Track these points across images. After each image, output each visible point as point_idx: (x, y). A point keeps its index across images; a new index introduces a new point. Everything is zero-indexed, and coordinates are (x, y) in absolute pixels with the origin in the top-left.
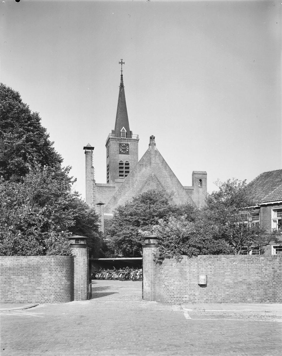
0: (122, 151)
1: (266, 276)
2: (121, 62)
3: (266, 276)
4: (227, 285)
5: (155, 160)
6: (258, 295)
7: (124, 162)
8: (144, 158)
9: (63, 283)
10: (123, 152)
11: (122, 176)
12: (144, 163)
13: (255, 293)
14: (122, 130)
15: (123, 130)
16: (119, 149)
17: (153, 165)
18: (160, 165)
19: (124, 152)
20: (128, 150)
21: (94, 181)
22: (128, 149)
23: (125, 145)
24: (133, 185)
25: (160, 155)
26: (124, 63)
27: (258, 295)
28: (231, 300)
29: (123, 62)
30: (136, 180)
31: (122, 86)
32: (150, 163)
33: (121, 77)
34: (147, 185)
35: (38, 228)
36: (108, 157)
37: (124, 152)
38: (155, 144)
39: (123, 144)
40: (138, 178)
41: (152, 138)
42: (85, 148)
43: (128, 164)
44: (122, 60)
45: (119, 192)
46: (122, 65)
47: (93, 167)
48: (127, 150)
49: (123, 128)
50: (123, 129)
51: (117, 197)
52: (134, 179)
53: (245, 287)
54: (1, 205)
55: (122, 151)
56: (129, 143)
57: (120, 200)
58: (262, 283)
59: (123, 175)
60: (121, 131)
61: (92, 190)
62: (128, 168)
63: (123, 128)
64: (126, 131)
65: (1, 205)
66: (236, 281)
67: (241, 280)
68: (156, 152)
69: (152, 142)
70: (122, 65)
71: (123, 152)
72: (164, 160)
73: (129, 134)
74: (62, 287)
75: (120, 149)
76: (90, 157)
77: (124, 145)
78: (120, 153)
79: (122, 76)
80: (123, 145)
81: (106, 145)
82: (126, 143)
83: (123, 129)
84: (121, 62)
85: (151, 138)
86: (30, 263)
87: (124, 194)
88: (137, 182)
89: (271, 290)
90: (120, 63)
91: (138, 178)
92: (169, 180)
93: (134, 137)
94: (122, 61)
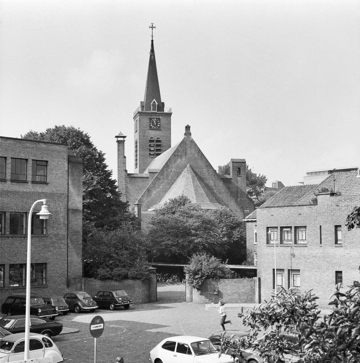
0: (153, 127)
2: (151, 26)
4: (228, 294)
5: (190, 152)
6: (244, 299)
8: (179, 149)
12: (179, 154)
13: (242, 298)
16: (149, 125)
17: (189, 155)
18: (196, 155)
21: (126, 171)
22: (159, 124)
24: (168, 177)
25: (196, 145)
26: (155, 27)
27: (244, 299)
29: (154, 26)
30: (171, 171)
32: (186, 153)
33: (151, 42)
37: (155, 127)
38: (190, 134)
40: (173, 170)
41: (188, 128)
42: (117, 137)
44: (152, 24)
45: (153, 184)
46: (152, 29)
47: (125, 157)
48: (159, 126)
49: (154, 100)
52: (169, 170)
53: (237, 295)
55: (153, 127)
56: (161, 118)
57: (155, 192)
58: (246, 293)
60: (151, 104)
61: (123, 181)
63: (154, 100)
64: (157, 104)
66: (233, 292)
68: (192, 141)
70: (152, 29)
71: (154, 127)
72: (200, 150)
73: (161, 106)
74: (145, 295)
76: (121, 147)
78: (151, 128)
79: (152, 41)
84: (151, 26)
85: (186, 127)
86: (129, 283)
87: (159, 187)
89: (250, 297)
90: (150, 27)
91: (173, 170)
92: (205, 170)
93: (166, 110)
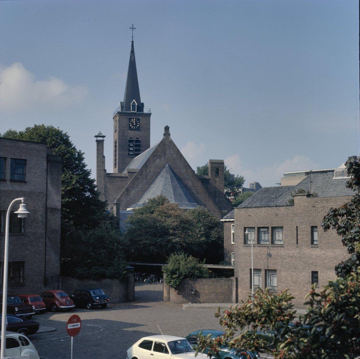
1: (225, 290)
2: (132, 27)
3: (225, 290)
9: (123, 292)
10: (133, 127)
14: (132, 102)
16: (128, 125)
19: (134, 128)
21: (105, 170)
22: (139, 125)
24: (147, 177)
28: (208, 301)
31: (133, 52)
34: (161, 177)
36: (115, 132)
40: (152, 169)
41: (167, 128)
42: (96, 136)
44: (133, 25)
46: (133, 30)
50: (133, 102)
51: (130, 189)
52: (148, 171)
56: (140, 118)
57: (133, 192)
63: (134, 100)
64: (137, 104)
67: (212, 291)
69: (166, 132)
70: (133, 30)
71: (133, 127)
73: (141, 107)
78: (130, 128)
79: (133, 42)
81: (113, 118)
83: (133, 102)
84: (132, 27)
88: (150, 174)
91: (152, 169)
93: (146, 111)
94: (133, 27)
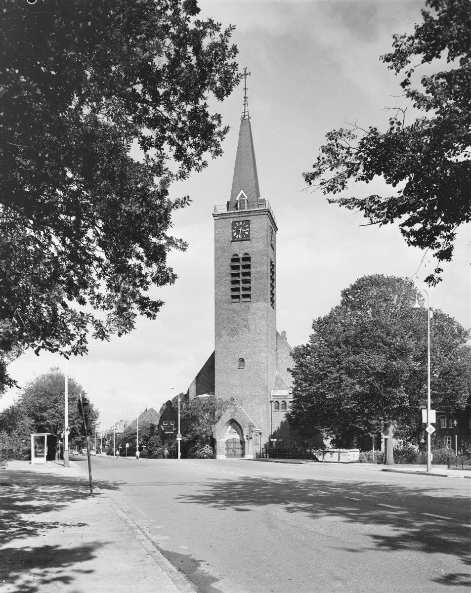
7: (241, 256)
11: (238, 297)
15: (242, 196)
20: (249, 231)
23: (243, 223)
26: (249, 74)
35: (441, 16)
39: (238, 222)
43: (249, 259)
49: (242, 192)
54: (468, 95)
59: (239, 266)
60: (238, 199)
62: (248, 267)
63: (242, 192)
64: (247, 198)
65: (468, 95)
75: (233, 233)
77: (241, 223)
80: (234, 232)
82: (245, 219)
